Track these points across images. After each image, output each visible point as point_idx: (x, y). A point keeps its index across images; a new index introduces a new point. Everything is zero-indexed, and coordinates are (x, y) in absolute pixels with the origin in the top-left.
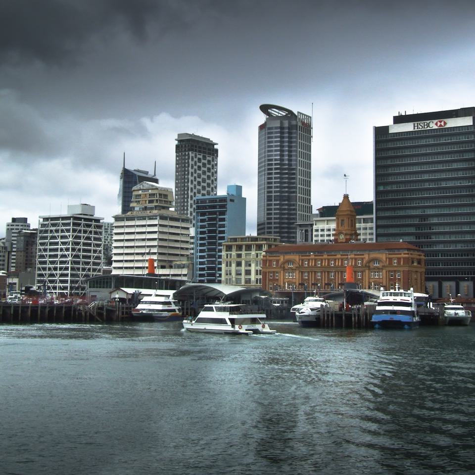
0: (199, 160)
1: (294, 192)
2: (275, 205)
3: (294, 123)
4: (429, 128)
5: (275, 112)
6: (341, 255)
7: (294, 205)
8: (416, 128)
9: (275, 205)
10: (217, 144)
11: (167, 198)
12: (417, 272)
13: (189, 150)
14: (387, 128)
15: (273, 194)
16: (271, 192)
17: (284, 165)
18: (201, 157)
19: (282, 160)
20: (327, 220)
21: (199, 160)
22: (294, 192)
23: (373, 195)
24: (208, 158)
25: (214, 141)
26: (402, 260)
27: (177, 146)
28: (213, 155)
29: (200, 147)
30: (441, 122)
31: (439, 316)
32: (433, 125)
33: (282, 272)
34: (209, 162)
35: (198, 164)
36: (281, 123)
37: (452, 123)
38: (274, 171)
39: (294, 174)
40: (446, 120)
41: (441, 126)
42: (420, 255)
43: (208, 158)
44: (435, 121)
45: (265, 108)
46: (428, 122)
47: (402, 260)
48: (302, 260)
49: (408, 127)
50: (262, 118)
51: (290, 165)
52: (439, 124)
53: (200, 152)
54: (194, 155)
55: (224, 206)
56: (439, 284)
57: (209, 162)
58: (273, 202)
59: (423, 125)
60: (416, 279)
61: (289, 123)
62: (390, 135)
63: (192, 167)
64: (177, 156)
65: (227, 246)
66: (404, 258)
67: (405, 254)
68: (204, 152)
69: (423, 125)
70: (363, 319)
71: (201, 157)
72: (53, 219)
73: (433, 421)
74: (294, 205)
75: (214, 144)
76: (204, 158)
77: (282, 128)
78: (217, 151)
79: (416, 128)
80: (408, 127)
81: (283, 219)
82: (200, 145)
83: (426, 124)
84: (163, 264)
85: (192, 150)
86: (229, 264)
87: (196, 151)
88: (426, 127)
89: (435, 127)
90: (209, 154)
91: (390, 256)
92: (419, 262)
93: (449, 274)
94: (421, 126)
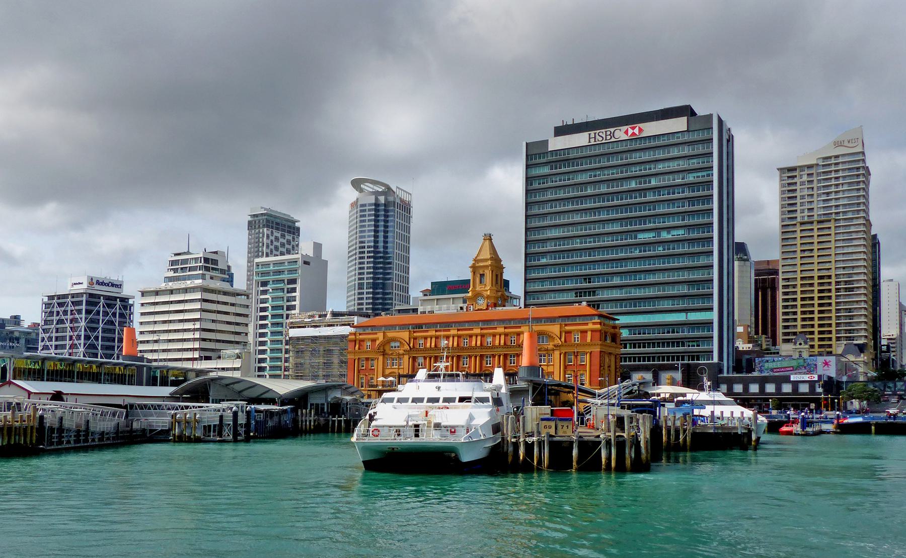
0: (277, 239)
1: (389, 279)
2: (367, 293)
3: (391, 199)
4: (613, 140)
5: (368, 187)
6: (482, 329)
7: (389, 293)
9: (367, 293)
10: (298, 221)
12: (610, 354)
13: (264, 226)
14: (545, 143)
15: (365, 281)
16: (362, 304)
17: (379, 252)
18: (279, 235)
19: (376, 247)
20: (437, 299)
21: (277, 239)
22: (389, 279)
23: (324, 449)
25: (296, 218)
26: (589, 334)
27: (250, 222)
28: (294, 234)
29: (277, 224)
30: (633, 128)
32: (621, 133)
33: (381, 358)
34: (289, 242)
35: (275, 243)
36: (377, 199)
37: (651, 128)
38: (367, 218)
39: (390, 268)
40: (641, 125)
41: (634, 134)
44: (624, 128)
45: (357, 184)
46: (612, 130)
47: (589, 334)
48: (415, 339)
49: (581, 139)
50: (352, 195)
51: (386, 253)
52: (630, 132)
53: (277, 229)
54: (269, 233)
56: (654, 377)
57: (289, 242)
58: (365, 291)
59: (604, 136)
61: (386, 199)
62: (549, 154)
63: (268, 247)
64: (249, 234)
66: (593, 331)
67: (594, 324)
68: (283, 230)
69: (604, 136)
70: (685, 439)
71: (279, 235)
72: (59, 297)
73: (299, 400)
74: (389, 293)
75: (294, 222)
76: (283, 236)
77: (377, 205)
78: (298, 229)
81: (376, 304)
82: (278, 221)
83: (608, 133)
84: (208, 354)
85: (268, 226)
87: (272, 228)
88: (609, 137)
89: (625, 137)
90: (289, 232)
91: (568, 328)
94: (601, 135)
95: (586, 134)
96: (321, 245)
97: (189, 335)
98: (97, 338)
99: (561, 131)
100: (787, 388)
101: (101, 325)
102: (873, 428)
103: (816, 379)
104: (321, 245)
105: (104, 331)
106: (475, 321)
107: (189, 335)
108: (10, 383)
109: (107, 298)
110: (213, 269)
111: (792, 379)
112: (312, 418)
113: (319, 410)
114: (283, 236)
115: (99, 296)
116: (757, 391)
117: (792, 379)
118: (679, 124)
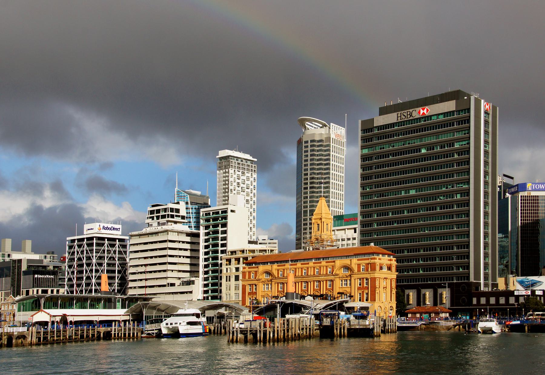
4: (411, 118)
8: (399, 118)
11: (179, 212)
24: (247, 175)
31: (373, 329)
35: (249, 182)
42: (390, 260)
43: (247, 175)
46: (411, 110)
49: (392, 118)
55: (225, 218)
59: (406, 115)
60: (385, 288)
65: (227, 260)
69: (406, 115)
79: (399, 118)
80: (392, 118)
83: (409, 113)
86: (228, 279)
88: (409, 116)
92: (389, 268)
93: (113, 262)
97: (182, 260)
99: (383, 111)
100: (512, 300)
101: (106, 261)
102: (526, 328)
103: (530, 293)
106: (309, 259)
107: (182, 260)
108: (42, 311)
109: (109, 239)
110: (176, 216)
111: (515, 294)
112: (113, 328)
114: (243, 173)
117: (515, 294)
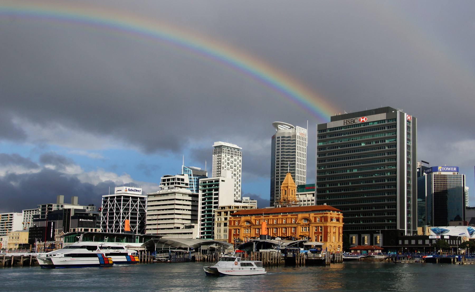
4: (354, 124)
12: (335, 227)
14: (326, 125)
30: (363, 118)
44: (359, 118)
46: (354, 119)
49: (340, 123)
52: (364, 119)
59: (348, 122)
94: (349, 121)
95: (342, 121)
96: (332, 117)
98: (137, 206)
101: (130, 211)
102: (437, 260)
104: (332, 117)
105: (132, 214)
110: (182, 183)
113: (204, 252)
114: (232, 157)
115: (129, 197)
116: (421, 243)
118: (383, 116)
